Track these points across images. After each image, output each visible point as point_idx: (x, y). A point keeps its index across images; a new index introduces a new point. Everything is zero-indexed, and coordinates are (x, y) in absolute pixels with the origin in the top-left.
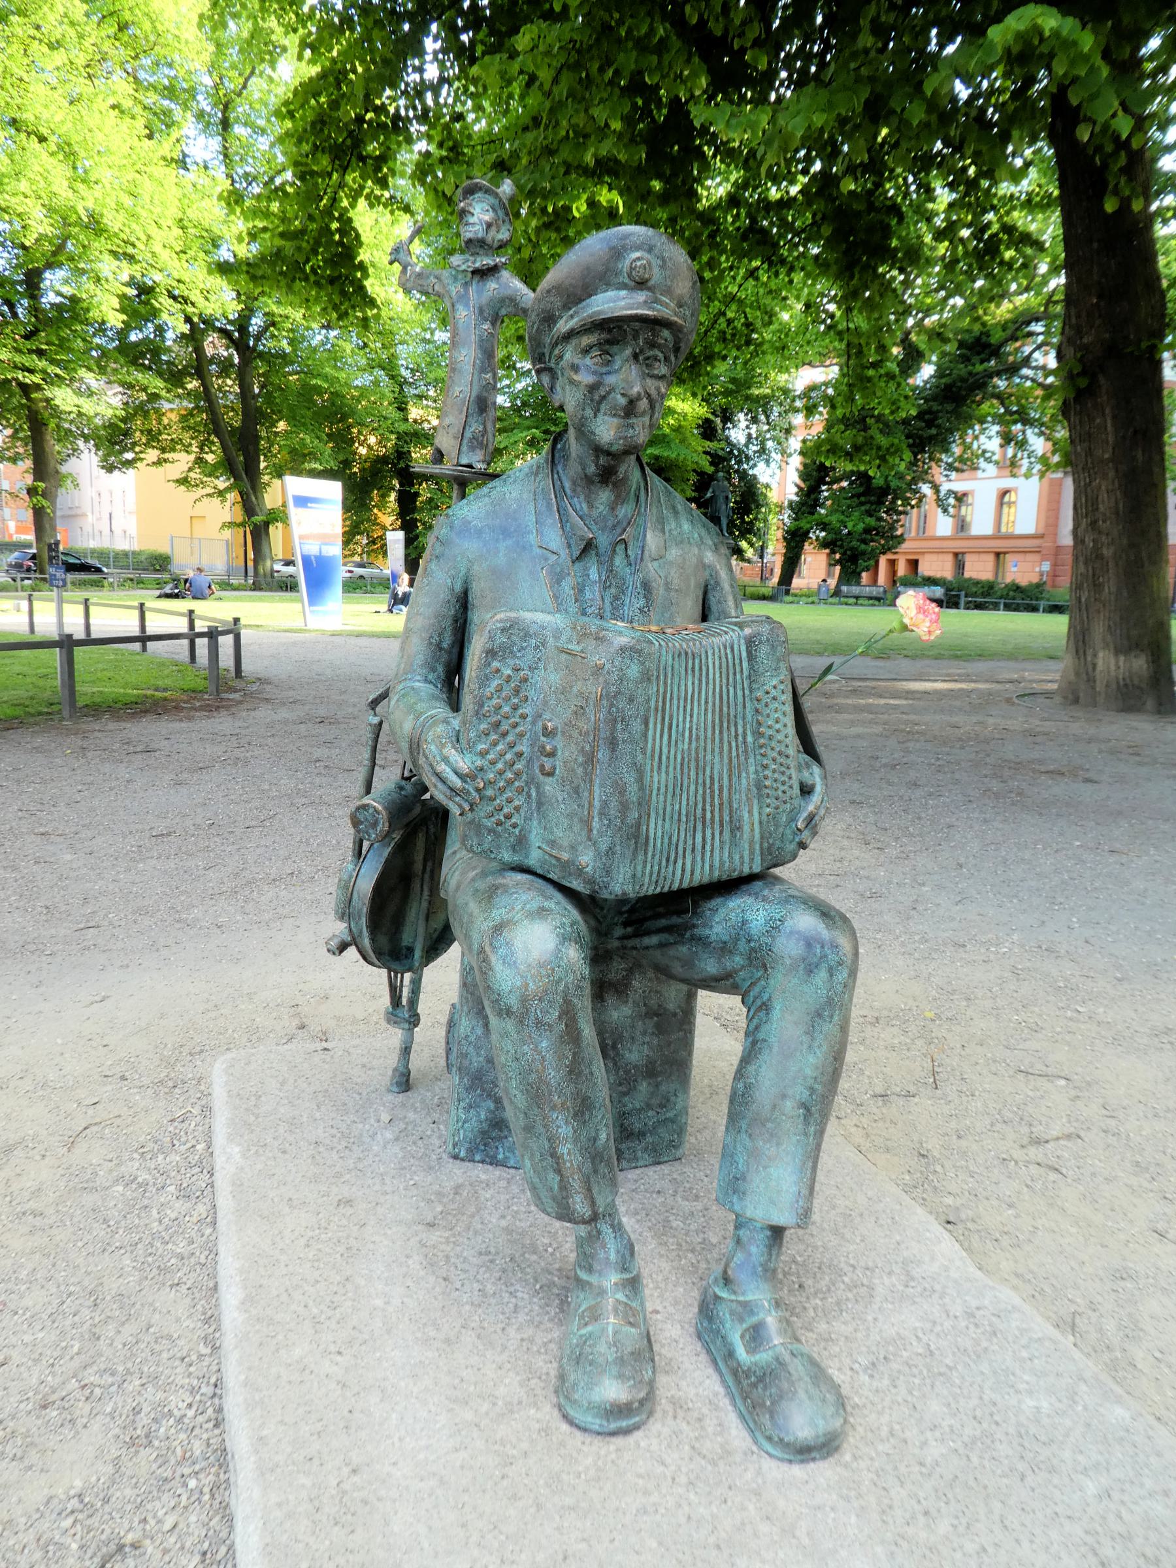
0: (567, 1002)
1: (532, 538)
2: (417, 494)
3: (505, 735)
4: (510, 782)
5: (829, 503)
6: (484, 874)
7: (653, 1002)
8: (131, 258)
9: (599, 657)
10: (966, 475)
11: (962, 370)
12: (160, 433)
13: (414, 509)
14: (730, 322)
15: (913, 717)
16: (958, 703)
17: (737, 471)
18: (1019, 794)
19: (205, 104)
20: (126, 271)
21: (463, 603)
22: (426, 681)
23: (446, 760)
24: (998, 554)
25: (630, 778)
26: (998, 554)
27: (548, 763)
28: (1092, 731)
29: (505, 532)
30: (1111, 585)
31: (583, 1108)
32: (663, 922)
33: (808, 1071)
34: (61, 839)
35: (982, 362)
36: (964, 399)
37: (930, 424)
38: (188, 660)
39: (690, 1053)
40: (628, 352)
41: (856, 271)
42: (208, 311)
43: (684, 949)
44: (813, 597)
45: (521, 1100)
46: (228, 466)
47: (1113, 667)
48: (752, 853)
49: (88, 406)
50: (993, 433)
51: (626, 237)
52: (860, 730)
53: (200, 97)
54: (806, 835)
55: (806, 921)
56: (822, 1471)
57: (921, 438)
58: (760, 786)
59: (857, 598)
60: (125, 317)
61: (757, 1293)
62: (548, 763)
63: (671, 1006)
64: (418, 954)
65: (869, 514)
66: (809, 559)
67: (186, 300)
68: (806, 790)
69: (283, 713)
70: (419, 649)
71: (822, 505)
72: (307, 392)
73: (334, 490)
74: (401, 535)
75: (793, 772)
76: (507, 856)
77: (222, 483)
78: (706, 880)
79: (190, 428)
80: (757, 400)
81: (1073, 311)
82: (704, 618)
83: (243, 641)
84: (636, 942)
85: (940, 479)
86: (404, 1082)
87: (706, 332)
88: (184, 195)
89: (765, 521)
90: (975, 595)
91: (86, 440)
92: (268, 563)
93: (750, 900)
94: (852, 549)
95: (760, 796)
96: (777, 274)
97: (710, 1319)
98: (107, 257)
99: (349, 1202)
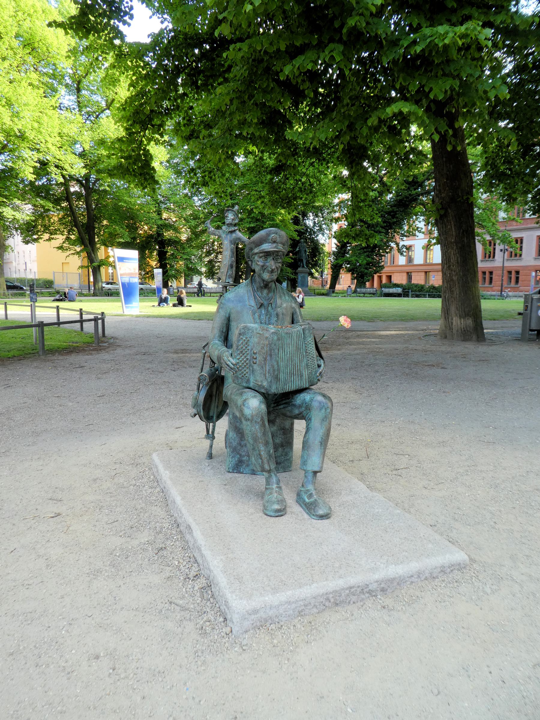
0: (262, 417)
1: (247, 303)
2: (167, 252)
3: (244, 354)
4: (245, 366)
5: (350, 252)
6: (238, 390)
7: (282, 426)
8: (38, 150)
9: (267, 335)
10: (411, 238)
11: (406, 193)
12: (50, 226)
13: (166, 259)
14: (303, 184)
15: (380, 346)
16: (399, 340)
17: (310, 239)
18: (416, 374)
19: (69, 81)
20: (36, 156)
21: (229, 320)
22: (219, 341)
23: (229, 361)
24: (426, 272)
25: (275, 363)
26: (426, 272)
27: (255, 361)
28: (449, 349)
29: (240, 301)
30: (457, 291)
31: (266, 444)
32: (284, 402)
33: (321, 434)
34: (65, 398)
35: (415, 189)
36: (408, 205)
37: (393, 217)
38: (80, 329)
39: (293, 441)
40: (272, 258)
41: (354, 165)
42: (73, 173)
43: (290, 408)
44: (345, 294)
45: (251, 441)
46: (81, 241)
47: (459, 324)
48: (306, 382)
49: (18, 215)
50: (421, 220)
51: (271, 231)
52: (358, 352)
53: (66, 78)
54: (319, 377)
55: (320, 398)
56: (326, 522)
57: (389, 223)
58: (307, 365)
59: (364, 294)
60: (35, 176)
61: (310, 487)
62: (255, 361)
63: (287, 427)
64: (215, 418)
65: (368, 256)
66: (343, 276)
67: (62, 168)
68: (319, 366)
69: (127, 351)
70: (217, 332)
71: (348, 253)
72: (117, 208)
73: (134, 254)
74: (160, 270)
75: (315, 361)
76: (245, 385)
77: (78, 249)
78: (295, 389)
79: (63, 224)
80: (317, 208)
81: (437, 184)
82: (293, 323)
83: (106, 323)
84: (277, 408)
85: (398, 240)
86: (210, 456)
87: (293, 188)
88: (62, 123)
89: (323, 260)
90: (415, 291)
91: (16, 231)
92: (100, 284)
93: (306, 394)
94: (361, 272)
95: (307, 368)
96: (322, 164)
97: (299, 496)
98: (27, 150)
99: (202, 481)
